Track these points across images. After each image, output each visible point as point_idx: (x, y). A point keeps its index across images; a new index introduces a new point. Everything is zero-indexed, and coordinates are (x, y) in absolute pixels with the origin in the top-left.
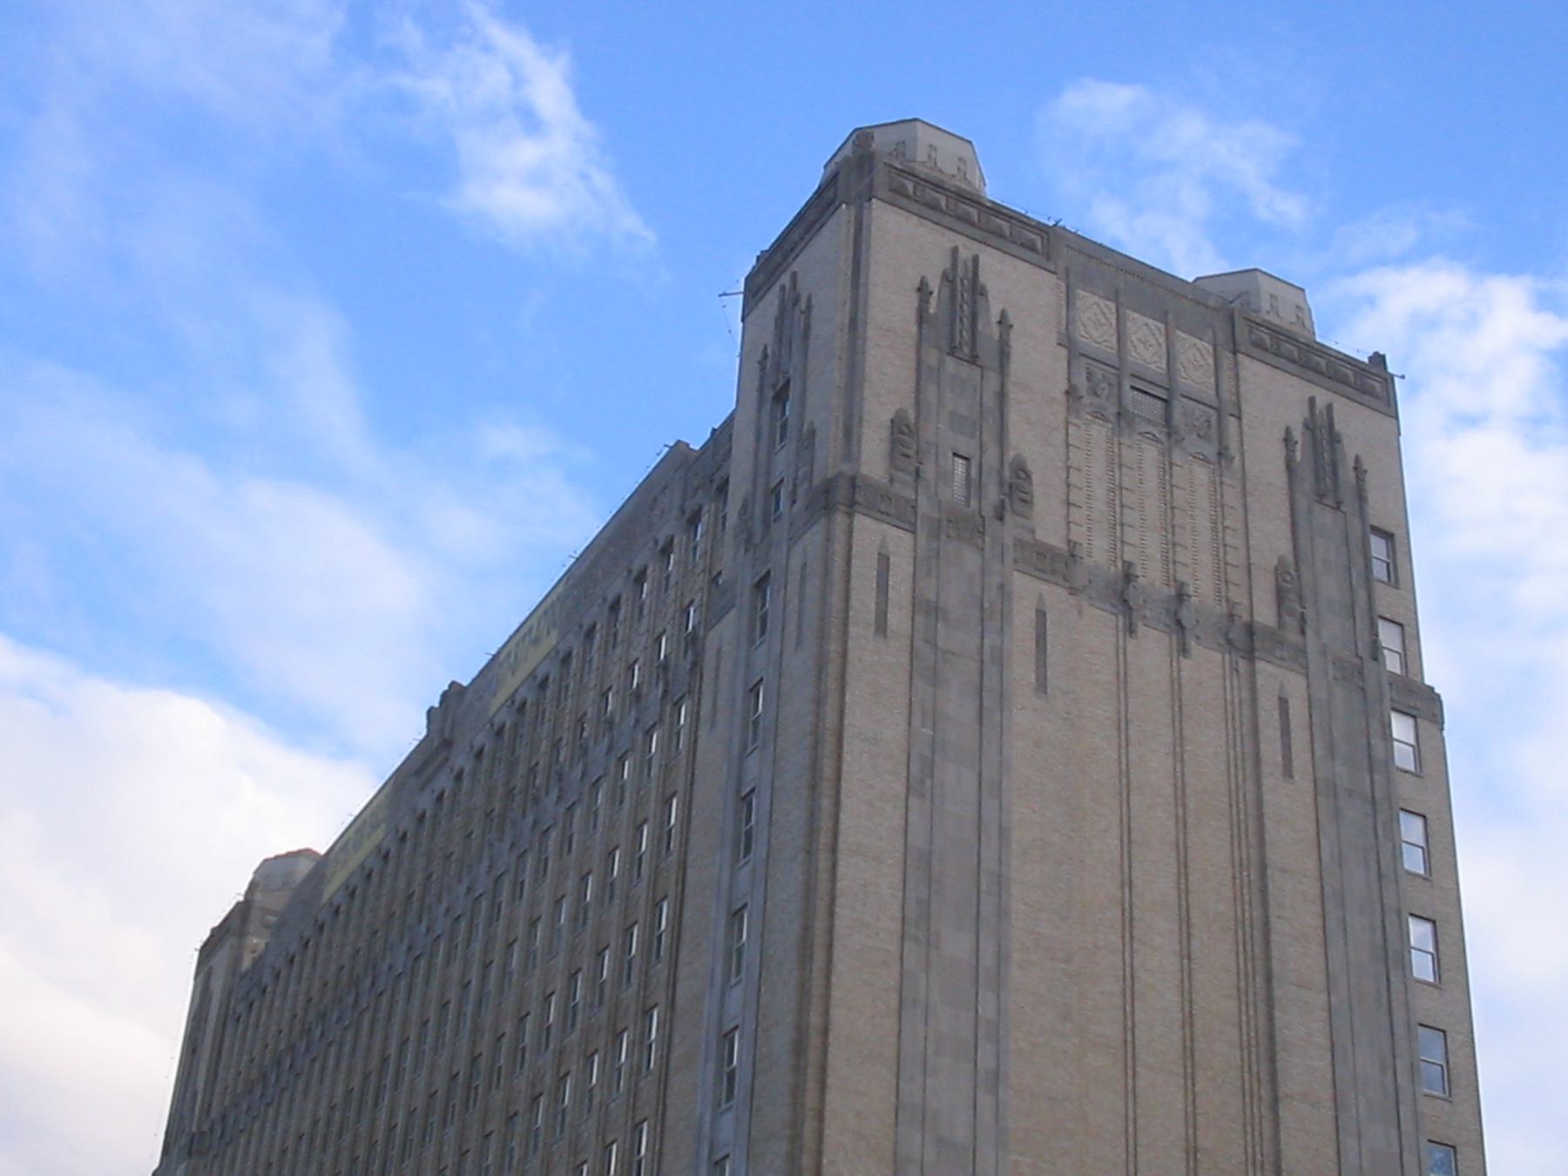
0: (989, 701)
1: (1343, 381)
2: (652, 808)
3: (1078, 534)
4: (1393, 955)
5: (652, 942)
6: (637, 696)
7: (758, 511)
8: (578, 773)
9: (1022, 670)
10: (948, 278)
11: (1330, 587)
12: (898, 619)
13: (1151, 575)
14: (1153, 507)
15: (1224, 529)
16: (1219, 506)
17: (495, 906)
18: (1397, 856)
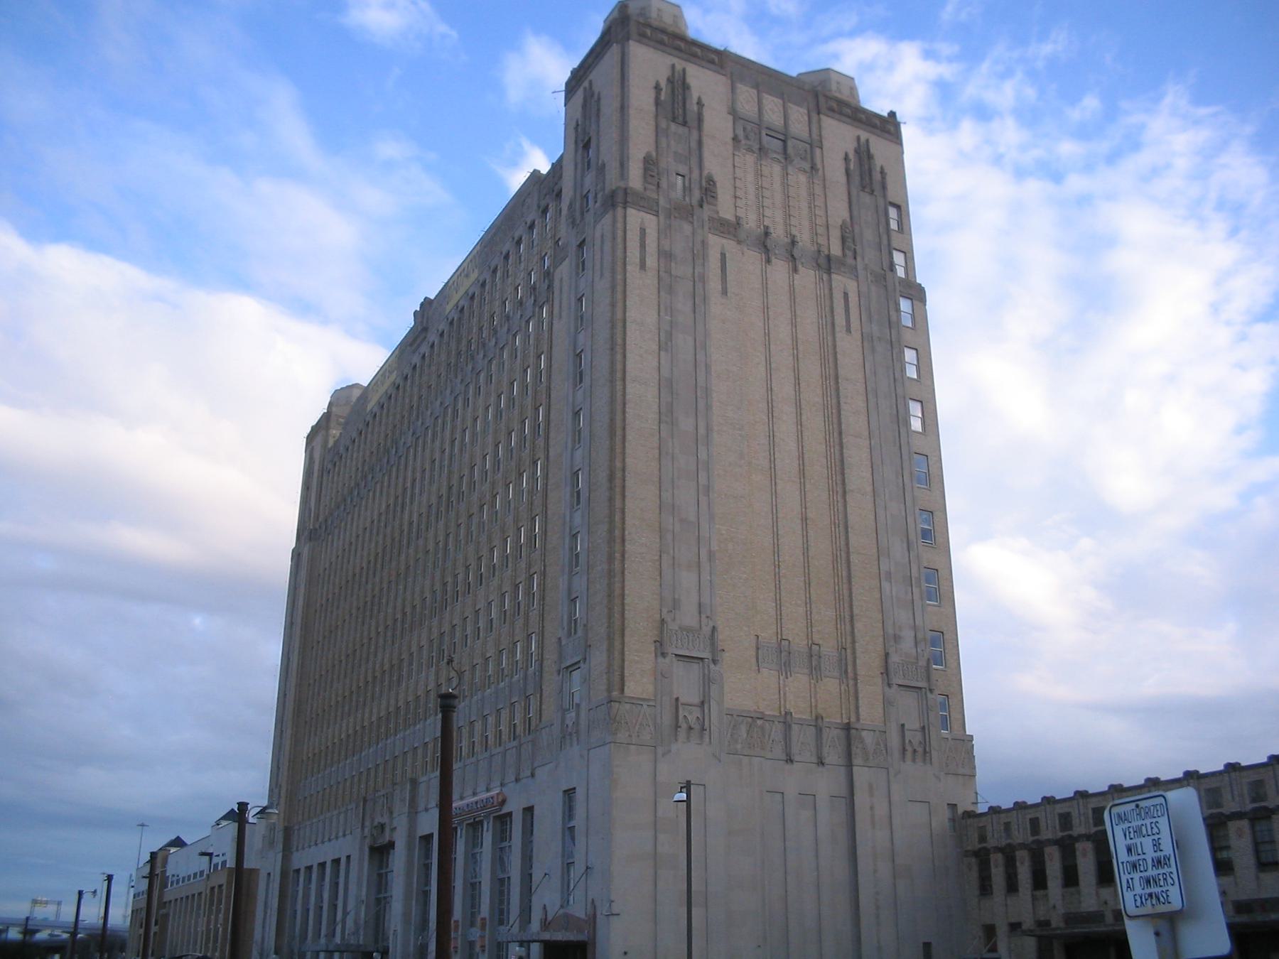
0: (698, 301)
1: (874, 126)
2: (532, 360)
3: (741, 213)
4: (901, 419)
5: (536, 427)
6: (521, 303)
7: (578, 204)
8: (493, 342)
9: (714, 284)
10: (670, 81)
11: (869, 235)
12: (651, 261)
13: (778, 232)
14: (779, 198)
15: (809, 206)
16: (812, 195)
17: (455, 412)
18: (903, 370)
